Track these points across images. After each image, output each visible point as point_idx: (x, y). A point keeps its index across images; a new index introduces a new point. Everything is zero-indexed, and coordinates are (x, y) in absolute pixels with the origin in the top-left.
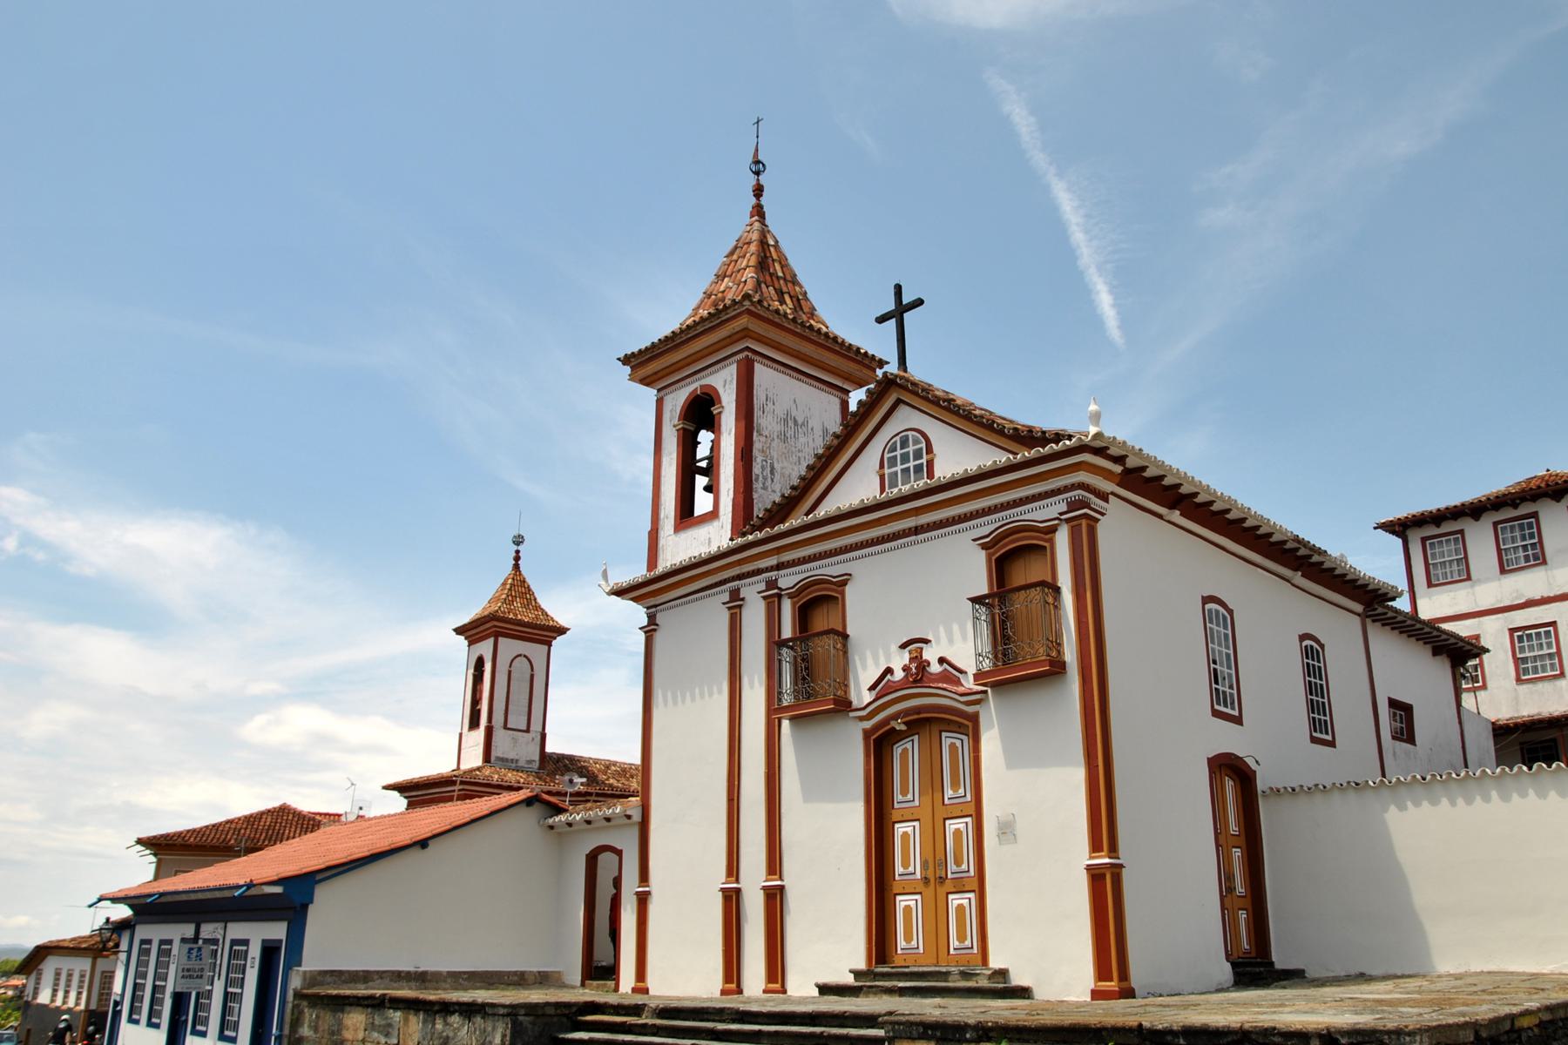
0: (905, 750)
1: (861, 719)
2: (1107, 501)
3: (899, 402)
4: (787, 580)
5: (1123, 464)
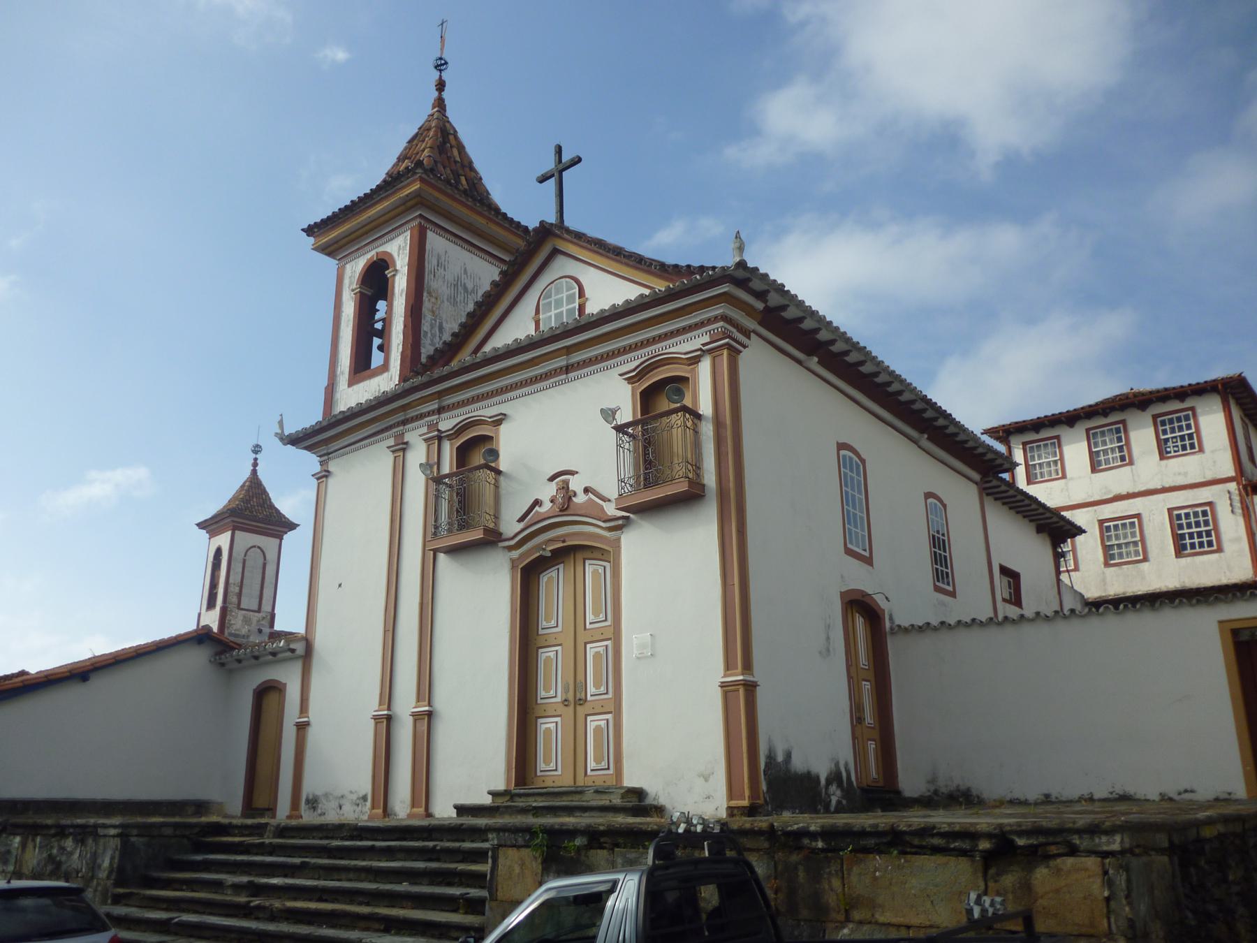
0: (551, 579)
1: (510, 548)
2: (749, 338)
3: (556, 252)
4: (446, 424)
5: (765, 301)
